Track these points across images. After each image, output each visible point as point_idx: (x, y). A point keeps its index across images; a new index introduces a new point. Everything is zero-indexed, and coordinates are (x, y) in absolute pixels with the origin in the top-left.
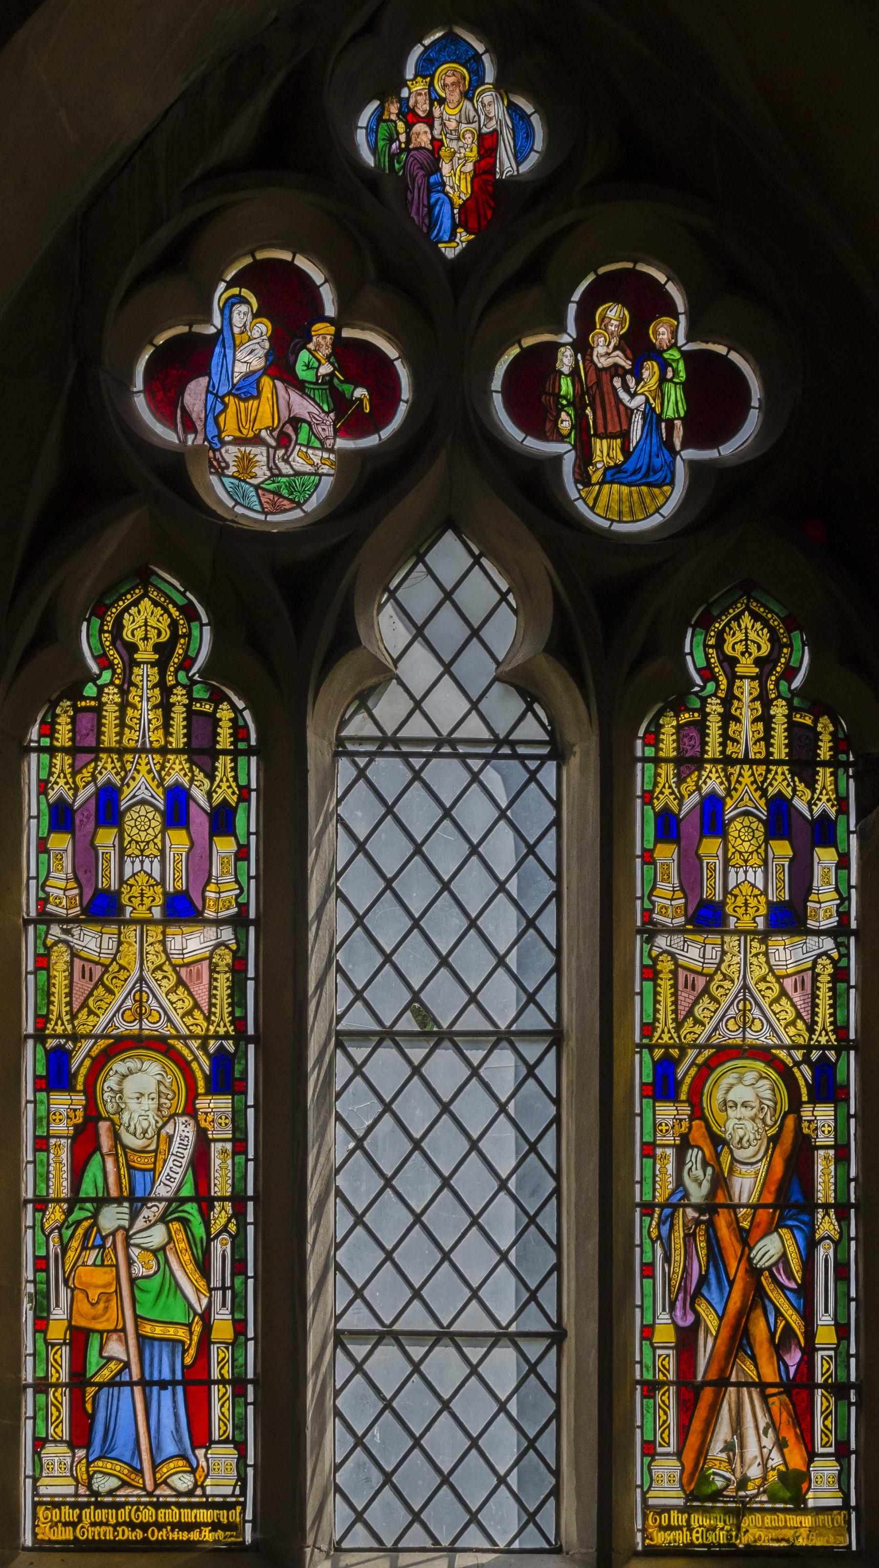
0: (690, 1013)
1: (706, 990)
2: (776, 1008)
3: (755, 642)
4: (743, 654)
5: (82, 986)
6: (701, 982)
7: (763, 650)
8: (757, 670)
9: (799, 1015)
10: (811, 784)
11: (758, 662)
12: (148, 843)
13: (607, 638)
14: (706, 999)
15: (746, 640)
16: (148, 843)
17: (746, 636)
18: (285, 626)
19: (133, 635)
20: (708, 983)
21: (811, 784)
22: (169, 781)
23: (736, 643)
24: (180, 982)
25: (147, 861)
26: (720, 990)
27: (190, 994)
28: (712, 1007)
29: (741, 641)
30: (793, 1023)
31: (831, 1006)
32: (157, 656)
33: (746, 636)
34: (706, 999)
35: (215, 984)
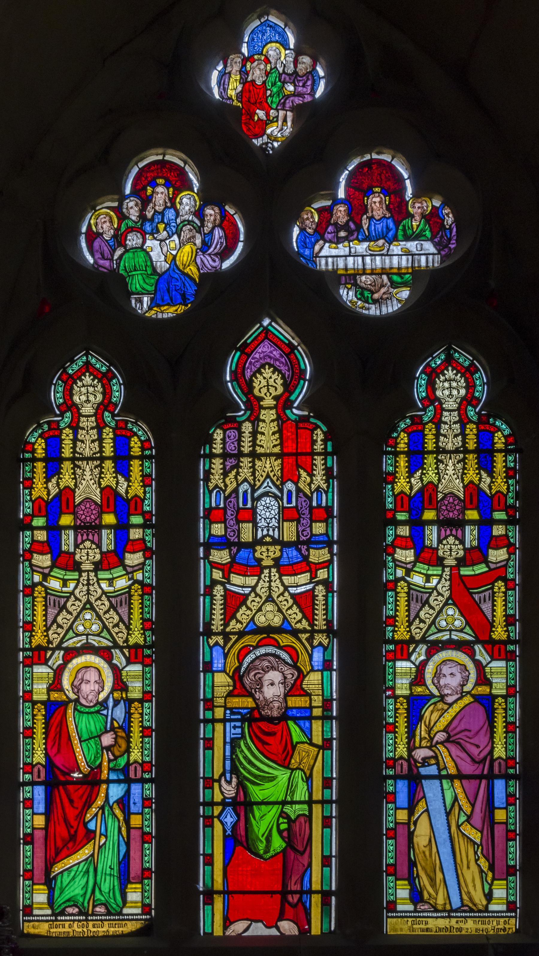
0: (55, 621)
1: (427, 602)
2: (107, 616)
3: (273, 386)
4: (85, 402)
5: (52, 612)
6: (63, 601)
7: (98, 399)
8: (275, 403)
9: (121, 620)
10: (127, 477)
11: (275, 398)
12: (271, 519)
13: (362, 382)
14: (64, 612)
15: (268, 385)
16: (271, 519)
17: (268, 383)
18: (177, 387)
19: (260, 392)
20: (66, 603)
21: (127, 477)
22: (104, 484)
23: (261, 388)
24: (112, 606)
25: (271, 529)
26: (73, 607)
27: (118, 613)
28: (431, 611)
29: (264, 386)
30: (117, 625)
31: (407, 611)
32: (275, 403)
33: (268, 383)
34: (64, 612)
35: (214, 607)
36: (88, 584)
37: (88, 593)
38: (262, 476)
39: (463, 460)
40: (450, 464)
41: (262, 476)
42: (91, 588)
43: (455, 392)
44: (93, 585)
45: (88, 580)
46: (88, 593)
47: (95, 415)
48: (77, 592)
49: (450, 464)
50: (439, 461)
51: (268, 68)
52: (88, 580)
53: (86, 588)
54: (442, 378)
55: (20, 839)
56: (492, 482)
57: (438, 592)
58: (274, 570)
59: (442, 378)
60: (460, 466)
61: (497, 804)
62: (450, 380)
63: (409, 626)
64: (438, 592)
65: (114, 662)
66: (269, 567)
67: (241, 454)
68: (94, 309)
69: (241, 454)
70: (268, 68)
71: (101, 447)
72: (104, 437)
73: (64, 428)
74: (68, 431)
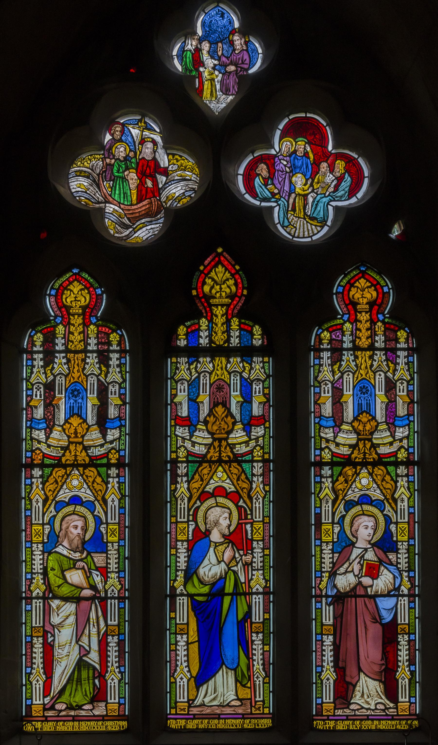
13: (289, 299)
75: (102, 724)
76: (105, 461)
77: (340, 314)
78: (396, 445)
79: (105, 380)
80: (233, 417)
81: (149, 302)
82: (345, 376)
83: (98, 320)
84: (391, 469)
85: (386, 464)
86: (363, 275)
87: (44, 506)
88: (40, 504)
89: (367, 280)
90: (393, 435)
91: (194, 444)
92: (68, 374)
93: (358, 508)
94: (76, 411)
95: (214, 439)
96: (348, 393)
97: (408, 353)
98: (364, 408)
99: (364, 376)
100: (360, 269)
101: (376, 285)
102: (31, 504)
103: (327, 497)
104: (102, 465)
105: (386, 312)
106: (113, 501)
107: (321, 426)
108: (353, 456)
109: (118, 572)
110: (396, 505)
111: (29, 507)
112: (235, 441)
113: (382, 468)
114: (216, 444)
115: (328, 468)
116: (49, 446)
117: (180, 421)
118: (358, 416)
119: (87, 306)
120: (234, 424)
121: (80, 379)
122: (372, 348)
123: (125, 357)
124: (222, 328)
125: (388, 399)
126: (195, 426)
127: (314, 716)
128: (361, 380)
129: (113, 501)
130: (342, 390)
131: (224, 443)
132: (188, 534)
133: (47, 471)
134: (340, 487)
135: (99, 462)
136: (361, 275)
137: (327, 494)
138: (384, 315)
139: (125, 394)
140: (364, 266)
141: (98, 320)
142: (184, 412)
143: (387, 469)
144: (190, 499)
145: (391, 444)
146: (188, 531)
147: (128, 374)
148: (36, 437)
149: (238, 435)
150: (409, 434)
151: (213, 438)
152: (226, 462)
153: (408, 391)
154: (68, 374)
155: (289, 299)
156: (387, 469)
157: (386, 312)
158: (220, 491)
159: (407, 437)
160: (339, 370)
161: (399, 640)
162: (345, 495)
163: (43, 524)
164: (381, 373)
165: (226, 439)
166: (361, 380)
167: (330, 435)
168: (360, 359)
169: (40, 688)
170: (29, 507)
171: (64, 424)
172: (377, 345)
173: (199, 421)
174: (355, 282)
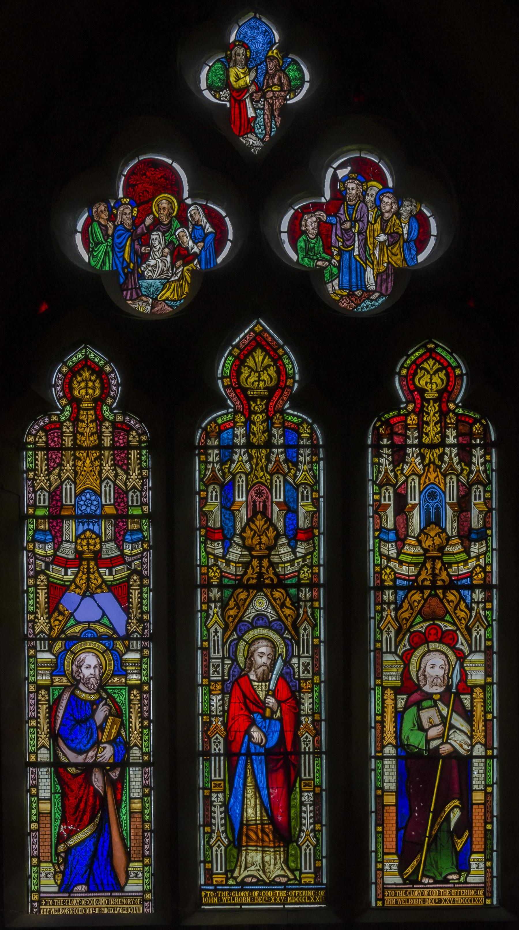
13: (347, 381)
36: (88, 572)
37: (88, 579)
38: (258, 472)
39: (99, 458)
40: (88, 461)
41: (258, 472)
42: (92, 576)
43: (90, 391)
44: (93, 573)
45: (88, 568)
46: (88, 579)
47: (94, 408)
48: (77, 580)
49: (88, 461)
50: (76, 458)
51: (250, 74)
52: (88, 568)
53: (85, 577)
54: (79, 379)
55: (430, 811)
56: (127, 479)
57: (76, 584)
58: (92, 563)
59: (79, 379)
60: (97, 463)
61: (475, 787)
62: (86, 381)
63: (49, 618)
64: (76, 584)
65: (458, 646)
66: (88, 560)
67: (61, 448)
68: (93, 307)
69: (61, 448)
70: (250, 74)
71: (100, 439)
72: (104, 430)
73: (65, 421)
74: (68, 423)
75: (259, 895)
76: (468, 581)
77: (403, 403)
78: (472, 563)
79: (294, 480)
80: (276, 529)
81: (168, 379)
82: (237, 478)
83: (457, 406)
84: (466, 593)
85: (458, 588)
86: (431, 354)
87: (396, 636)
88: (393, 634)
89: (437, 361)
90: (294, 552)
91: (228, 563)
92: (250, 473)
93: (242, 643)
94: (433, 519)
95: (253, 557)
96: (241, 499)
97: (312, 451)
98: (433, 519)
99: (432, 481)
100: (426, 348)
101: (445, 367)
102: (208, 635)
103: (389, 625)
104: (292, 586)
105: (458, 400)
106: (216, 632)
107: (381, 540)
108: (420, 578)
109: (313, 715)
110: (470, 635)
111: (378, 636)
112: (451, 558)
113: (454, 592)
114: (255, 563)
115: (480, 591)
116: (401, 563)
117: (211, 535)
118: (425, 528)
119: (445, 390)
120: (278, 536)
121: (437, 480)
122: (269, 445)
123: (490, 454)
124: (434, 418)
125: (487, 507)
126: (232, 538)
127: (201, 885)
128: (427, 486)
129: (216, 632)
130: (406, 496)
131: (265, 563)
132: (223, 672)
133: (227, 592)
134: (406, 615)
135: (460, 583)
136: (428, 354)
137: (389, 622)
138: (455, 404)
139: (491, 499)
140: (431, 342)
141: (457, 406)
142: (215, 522)
143: (460, 594)
144: (225, 631)
145: (465, 562)
146: (223, 669)
147: (494, 473)
148: (386, 553)
149: (284, 551)
150: (487, 551)
151: (250, 555)
152: (267, 586)
153: (485, 499)
154: (250, 473)
155: (347, 381)
156: (460, 594)
157: (458, 400)
158: (260, 620)
159: (485, 554)
160: (402, 473)
161: (213, 799)
162: (411, 626)
163: (223, 659)
164: (242, 475)
165: (268, 556)
166: (427, 486)
167: (393, 552)
168: (255, 460)
169: (221, 854)
170: (378, 636)
171: (419, 535)
172: (275, 441)
173: (235, 534)
174: (422, 363)
